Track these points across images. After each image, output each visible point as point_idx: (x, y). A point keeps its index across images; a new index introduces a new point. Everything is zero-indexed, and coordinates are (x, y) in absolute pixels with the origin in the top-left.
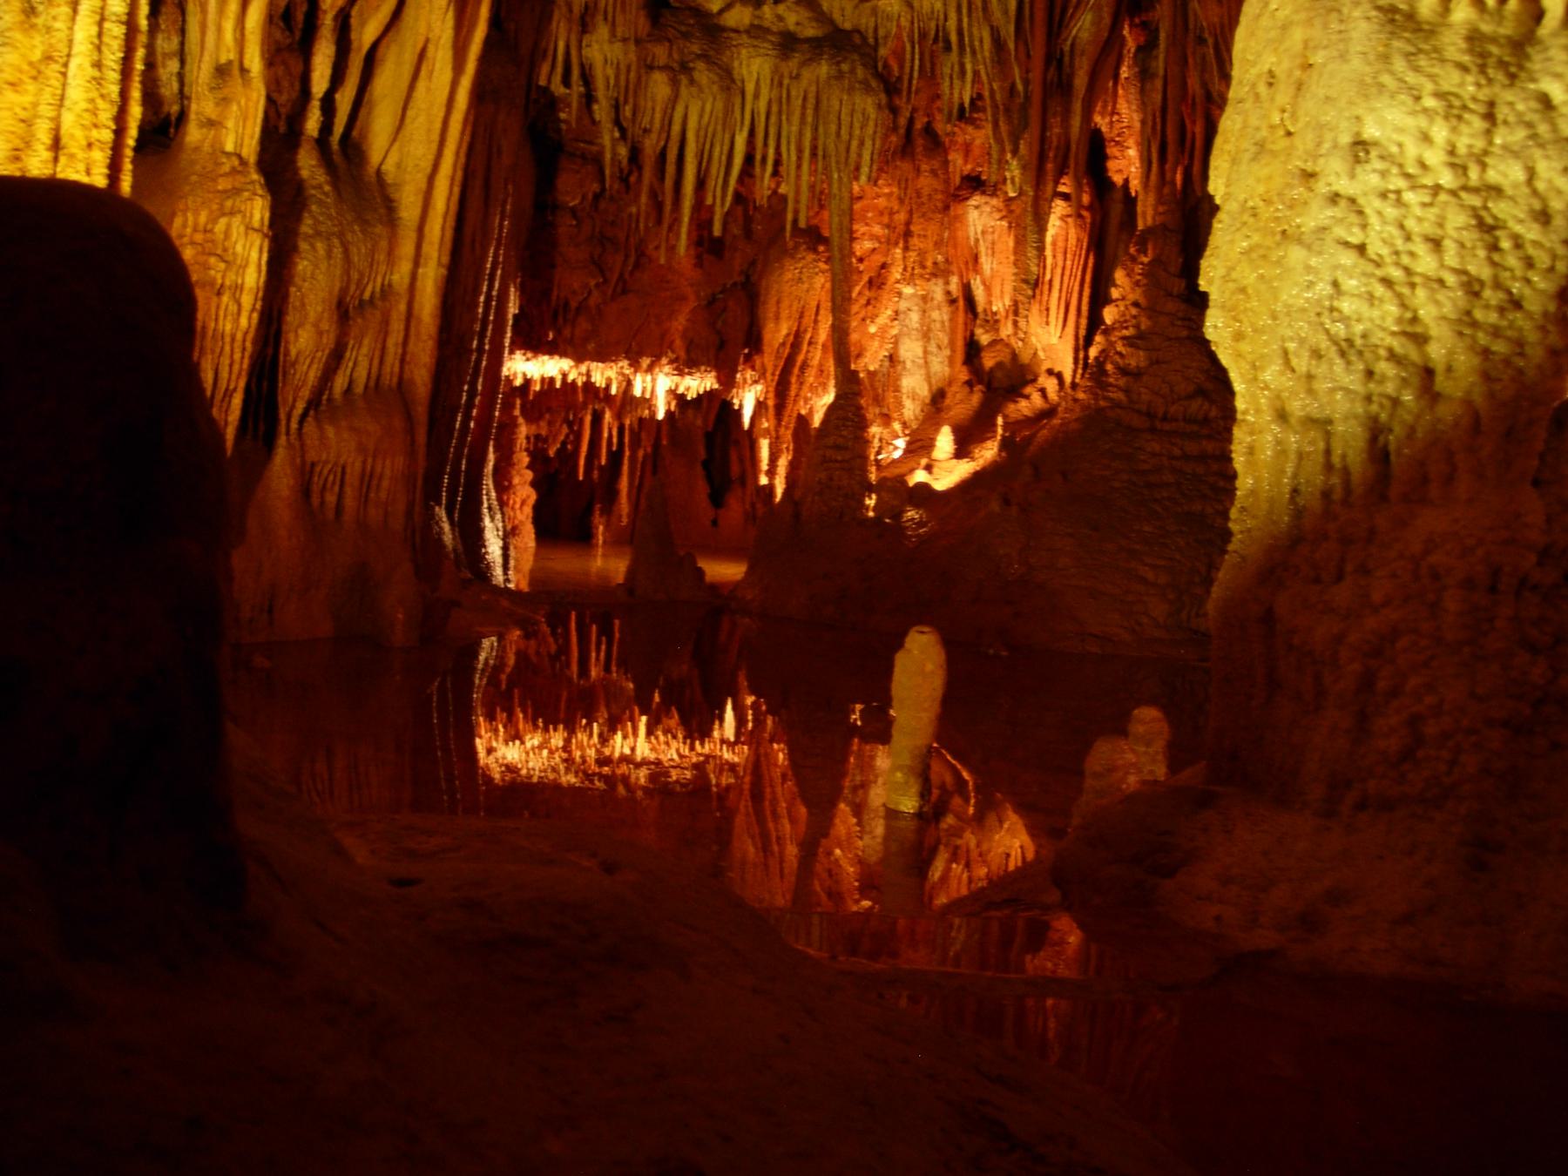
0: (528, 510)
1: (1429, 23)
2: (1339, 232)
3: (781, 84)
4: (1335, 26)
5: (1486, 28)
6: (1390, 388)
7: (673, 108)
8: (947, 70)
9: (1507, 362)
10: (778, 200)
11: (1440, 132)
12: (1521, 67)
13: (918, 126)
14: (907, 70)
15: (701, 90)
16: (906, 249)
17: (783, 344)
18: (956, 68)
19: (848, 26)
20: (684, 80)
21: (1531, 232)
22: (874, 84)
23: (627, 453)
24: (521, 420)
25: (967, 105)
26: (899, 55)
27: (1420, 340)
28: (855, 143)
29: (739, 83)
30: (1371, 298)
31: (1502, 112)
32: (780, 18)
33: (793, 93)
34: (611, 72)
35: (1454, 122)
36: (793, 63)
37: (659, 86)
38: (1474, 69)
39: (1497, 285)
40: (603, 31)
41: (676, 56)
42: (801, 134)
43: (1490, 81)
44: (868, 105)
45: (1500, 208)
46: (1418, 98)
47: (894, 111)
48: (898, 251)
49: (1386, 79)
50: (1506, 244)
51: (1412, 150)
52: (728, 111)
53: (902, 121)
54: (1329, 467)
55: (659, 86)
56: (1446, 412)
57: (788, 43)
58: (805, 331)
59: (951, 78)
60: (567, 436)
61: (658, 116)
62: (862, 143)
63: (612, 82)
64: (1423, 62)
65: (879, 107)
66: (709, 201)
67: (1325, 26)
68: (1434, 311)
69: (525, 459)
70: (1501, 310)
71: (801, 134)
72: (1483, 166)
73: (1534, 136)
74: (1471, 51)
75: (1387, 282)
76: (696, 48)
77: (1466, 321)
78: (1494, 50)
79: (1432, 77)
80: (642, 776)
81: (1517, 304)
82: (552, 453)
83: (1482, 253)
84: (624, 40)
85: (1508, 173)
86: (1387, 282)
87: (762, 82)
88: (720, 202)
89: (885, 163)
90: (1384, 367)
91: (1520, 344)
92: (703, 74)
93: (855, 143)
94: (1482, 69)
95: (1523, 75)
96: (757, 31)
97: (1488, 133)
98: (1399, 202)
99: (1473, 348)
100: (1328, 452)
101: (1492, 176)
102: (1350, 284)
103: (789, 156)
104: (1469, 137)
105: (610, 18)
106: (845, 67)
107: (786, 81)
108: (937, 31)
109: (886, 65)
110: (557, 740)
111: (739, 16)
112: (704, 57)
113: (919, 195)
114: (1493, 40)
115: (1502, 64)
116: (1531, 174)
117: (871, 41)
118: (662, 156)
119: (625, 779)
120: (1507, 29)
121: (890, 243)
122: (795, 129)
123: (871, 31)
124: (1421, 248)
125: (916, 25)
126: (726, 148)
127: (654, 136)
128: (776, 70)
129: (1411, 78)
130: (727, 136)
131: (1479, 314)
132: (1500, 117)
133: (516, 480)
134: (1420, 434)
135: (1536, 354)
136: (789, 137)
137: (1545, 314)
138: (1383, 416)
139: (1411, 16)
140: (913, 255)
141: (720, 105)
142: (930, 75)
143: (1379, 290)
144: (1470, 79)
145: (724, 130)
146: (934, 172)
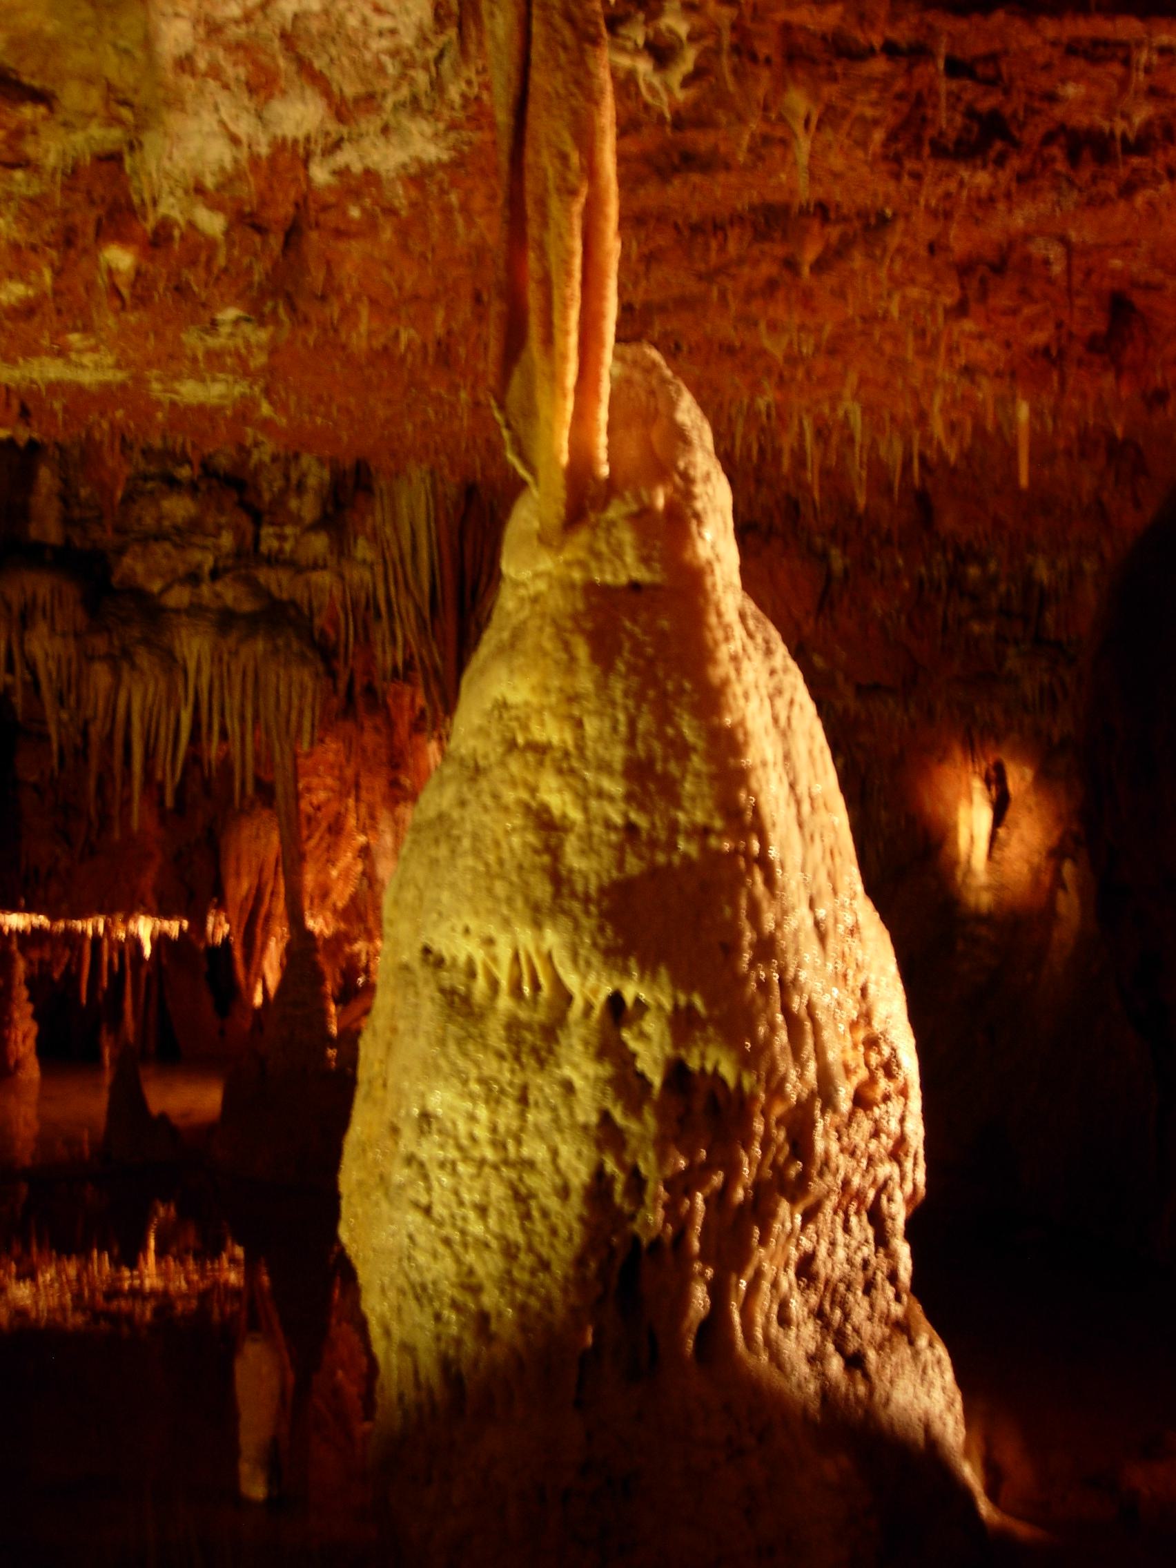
0: (31, 1042)
1: (480, 1007)
2: (411, 1193)
3: (221, 660)
4: (412, 999)
5: (523, 1015)
6: (454, 1330)
7: (117, 694)
8: (379, 637)
9: (539, 1316)
10: (226, 764)
11: (482, 1113)
12: (551, 1051)
13: (358, 688)
14: (343, 637)
15: (142, 673)
16: (358, 799)
17: (246, 898)
18: (387, 634)
19: (285, 596)
20: (125, 667)
21: (553, 1203)
22: (310, 655)
23: (129, 972)
24: (18, 955)
25: (400, 664)
26: (334, 623)
27: (475, 1290)
28: (294, 716)
29: (181, 662)
30: (435, 1255)
31: (533, 1096)
32: (218, 596)
33: (233, 668)
34: (52, 666)
35: (493, 1104)
36: (231, 641)
37: (101, 676)
38: (509, 1056)
39: (531, 1249)
40: (43, 628)
41: (116, 643)
42: (243, 706)
43: (522, 1067)
44: (305, 677)
45: (532, 1181)
46: (465, 1082)
47: (332, 674)
48: (351, 802)
49: (443, 1063)
50: (536, 1214)
51: (462, 1128)
52: (171, 690)
53: (342, 686)
54: (417, 1384)
55: (101, 676)
56: (500, 1352)
57: (226, 620)
58: (267, 883)
59: (383, 644)
60: (70, 960)
61: (101, 704)
62: (301, 713)
63: (54, 675)
64: (471, 1047)
65: (317, 675)
66: (159, 775)
67: (405, 998)
68: (488, 1266)
69: (24, 993)
70: (533, 1273)
71: (243, 706)
72: (519, 1142)
73: (556, 1120)
74: (509, 1040)
75: (447, 1242)
76: (136, 633)
77: (507, 1281)
78: (528, 1036)
79: (477, 1064)
80: (147, 1312)
81: (545, 1265)
82: (56, 976)
83: (516, 1221)
84: (64, 635)
85: (535, 1150)
86: (447, 1242)
87: (203, 661)
88: (170, 775)
89: (325, 725)
90: (450, 1315)
91: (548, 1303)
92: (144, 659)
93: (294, 716)
94: (517, 1058)
95: (551, 1060)
96: (195, 610)
97: (522, 1116)
98: (454, 1172)
99: (512, 1303)
100: (416, 1373)
101: (526, 1152)
102: (421, 1239)
103: (233, 726)
104: (507, 1116)
105: (48, 613)
106: (280, 642)
107: (226, 657)
108: (368, 598)
109: (323, 633)
110: (72, 1271)
111: (179, 597)
112: (146, 642)
113: (364, 750)
114: (528, 1027)
115: (535, 1051)
116: (555, 1153)
117: (306, 611)
118: (110, 738)
119: (129, 1317)
120: (541, 1016)
121: (342, 795)
122: (237, 703)
123: (305, 602)
124: (472, 1215)
125: (348, 593)
126: (172, 726)
127: (99, 723)
128: (215, 649)
129: (461, 1063)
130: (172, 713)
131: (516, 1274)
132: (531, 1099)
133: (17, 1015)
134: (481, 1365)
135: (560, 1310)
136: (232, 709)
137: (566, 1278)
138: (452, 1352)
139: (466, 999)
140: (363, 810)
141: (162, 686)
142: (365, 640)
143: (441, 1249)
144: (506, 1065)
145: (168, 710)
146: (377, 730)
